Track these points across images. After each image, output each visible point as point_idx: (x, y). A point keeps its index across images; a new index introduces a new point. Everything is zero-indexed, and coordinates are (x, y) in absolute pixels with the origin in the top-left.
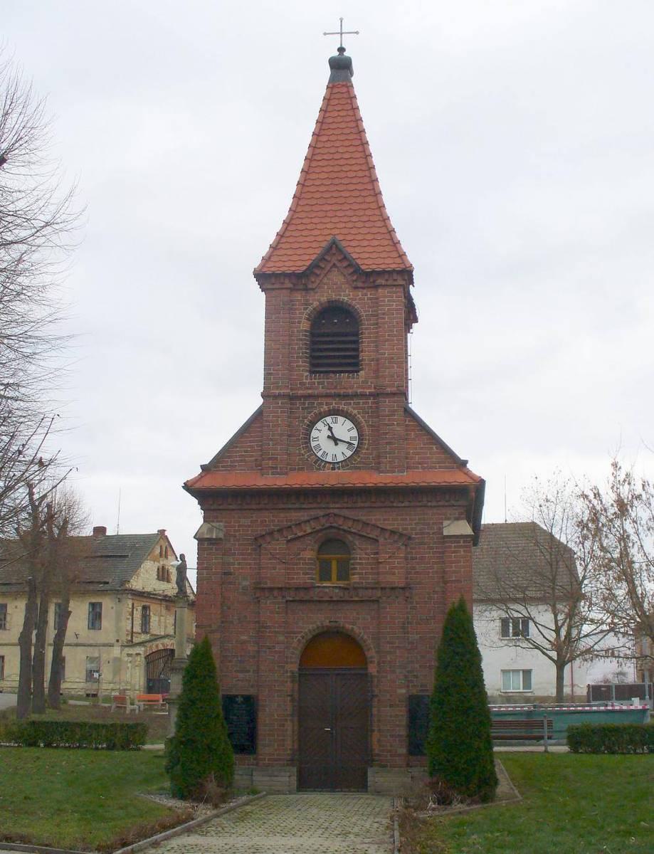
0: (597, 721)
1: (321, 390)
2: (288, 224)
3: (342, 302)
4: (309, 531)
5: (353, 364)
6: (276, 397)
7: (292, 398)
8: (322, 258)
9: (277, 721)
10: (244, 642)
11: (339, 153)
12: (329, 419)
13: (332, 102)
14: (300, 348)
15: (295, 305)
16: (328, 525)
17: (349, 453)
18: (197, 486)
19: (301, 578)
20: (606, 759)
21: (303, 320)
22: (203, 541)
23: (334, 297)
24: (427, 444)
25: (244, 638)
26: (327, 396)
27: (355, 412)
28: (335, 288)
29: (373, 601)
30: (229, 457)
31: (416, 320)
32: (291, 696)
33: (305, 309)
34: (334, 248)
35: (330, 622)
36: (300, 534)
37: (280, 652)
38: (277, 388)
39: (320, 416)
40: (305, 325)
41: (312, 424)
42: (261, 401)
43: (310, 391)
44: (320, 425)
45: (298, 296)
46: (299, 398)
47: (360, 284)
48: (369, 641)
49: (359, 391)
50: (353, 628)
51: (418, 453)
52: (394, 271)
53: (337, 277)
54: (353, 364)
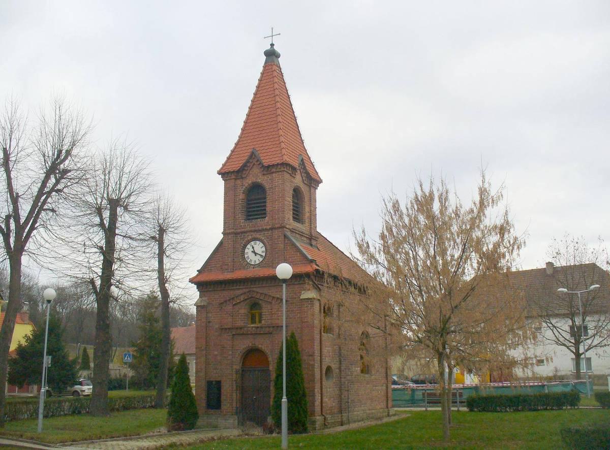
0: (494, 393)
1: (248, 229)
2: (237, 145)
3: (258, 183)
4: (242, 300)
5: (262, 213)
6: (229, 234)
7: (236, 234)
8: (248, 162)
9: (230, 395)
10: (216, 355)
11: (271, 103)
12: (252, 243)
13: (264, 75)
14: (239, 208)
15: (237, 186)
16: (250, 296)
17: (261, 259)
18: (195, 280)
19: (240, 323)
20: (489, 416)
21: (241, 194)
22: (199, 307)
23: (254, 180)
24: (295, 252)
25: (216, 353)
26: (251, 231)
27: (263, 238)
28: (255, 176)
29: (269, 333)
30: (210, 265)
31: (318, 181)
32: (236, 381)
33: (242, 188)
34: (252, 155)
35: (252, 344)
36: (238, 301)
37: (230, 360)
38: (229, 229)
39: (249, 242)
40: (242, 196)
41: (245, 247)
42: (222, 236)
43: (243, 230)
44: (249, 246)
45: (239, 182)
46: (239, 233)
47: (265, 173)
48: (269, 353)
49: (265, 227)
50: (261, 347)
51: (291, 257)
52: (278, 164)
53: (256, 170)
54: (262, 213)
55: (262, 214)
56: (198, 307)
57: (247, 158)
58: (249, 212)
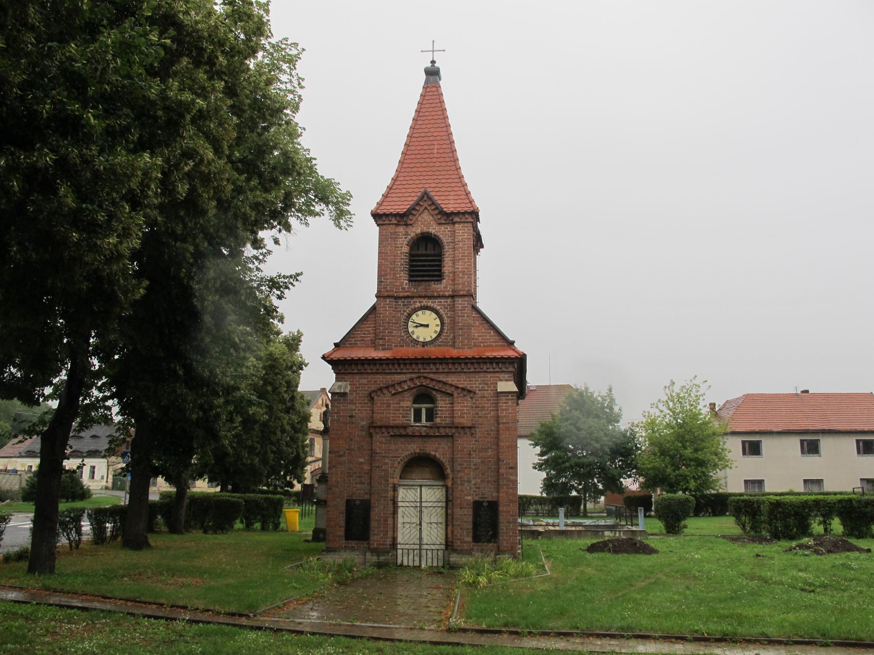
4: (406, 388)
10: (362, 463)
23: (425, 230)
25: (362, 460)
28: (425, 223)
45: (401, 229)
46: (401, 298)
53: (426, 217)
55: (435, 276)
56: (333, 394)
57: (415, 199)
58: (437, 266)
